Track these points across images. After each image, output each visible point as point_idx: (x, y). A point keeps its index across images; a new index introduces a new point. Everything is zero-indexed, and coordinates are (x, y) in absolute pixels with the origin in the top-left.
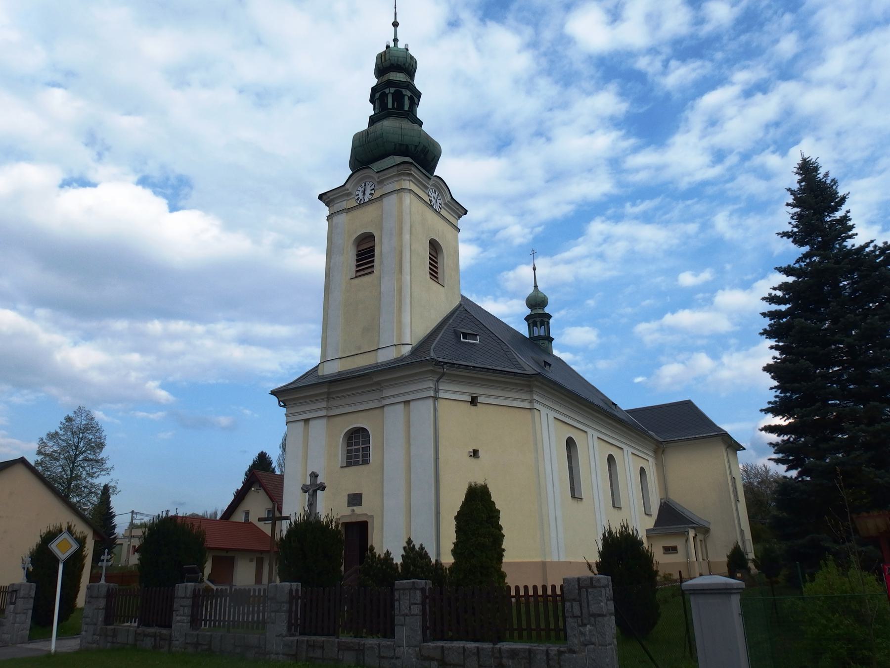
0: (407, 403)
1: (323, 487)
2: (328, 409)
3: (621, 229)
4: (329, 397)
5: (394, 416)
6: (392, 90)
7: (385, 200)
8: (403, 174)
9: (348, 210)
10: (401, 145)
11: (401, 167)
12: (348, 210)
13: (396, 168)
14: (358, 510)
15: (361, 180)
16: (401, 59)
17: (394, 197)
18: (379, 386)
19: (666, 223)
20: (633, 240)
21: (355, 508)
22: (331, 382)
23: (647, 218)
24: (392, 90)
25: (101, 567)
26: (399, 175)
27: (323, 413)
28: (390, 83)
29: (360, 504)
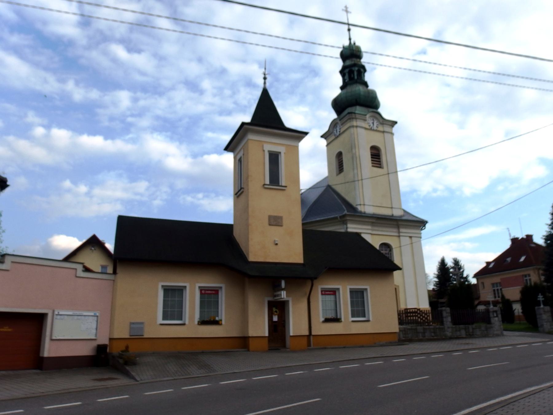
0: (411, 237)
4: (373, 224)
9: (366, 129)
12: (366, 129)
19: (36, 65)
23: (16, 51)
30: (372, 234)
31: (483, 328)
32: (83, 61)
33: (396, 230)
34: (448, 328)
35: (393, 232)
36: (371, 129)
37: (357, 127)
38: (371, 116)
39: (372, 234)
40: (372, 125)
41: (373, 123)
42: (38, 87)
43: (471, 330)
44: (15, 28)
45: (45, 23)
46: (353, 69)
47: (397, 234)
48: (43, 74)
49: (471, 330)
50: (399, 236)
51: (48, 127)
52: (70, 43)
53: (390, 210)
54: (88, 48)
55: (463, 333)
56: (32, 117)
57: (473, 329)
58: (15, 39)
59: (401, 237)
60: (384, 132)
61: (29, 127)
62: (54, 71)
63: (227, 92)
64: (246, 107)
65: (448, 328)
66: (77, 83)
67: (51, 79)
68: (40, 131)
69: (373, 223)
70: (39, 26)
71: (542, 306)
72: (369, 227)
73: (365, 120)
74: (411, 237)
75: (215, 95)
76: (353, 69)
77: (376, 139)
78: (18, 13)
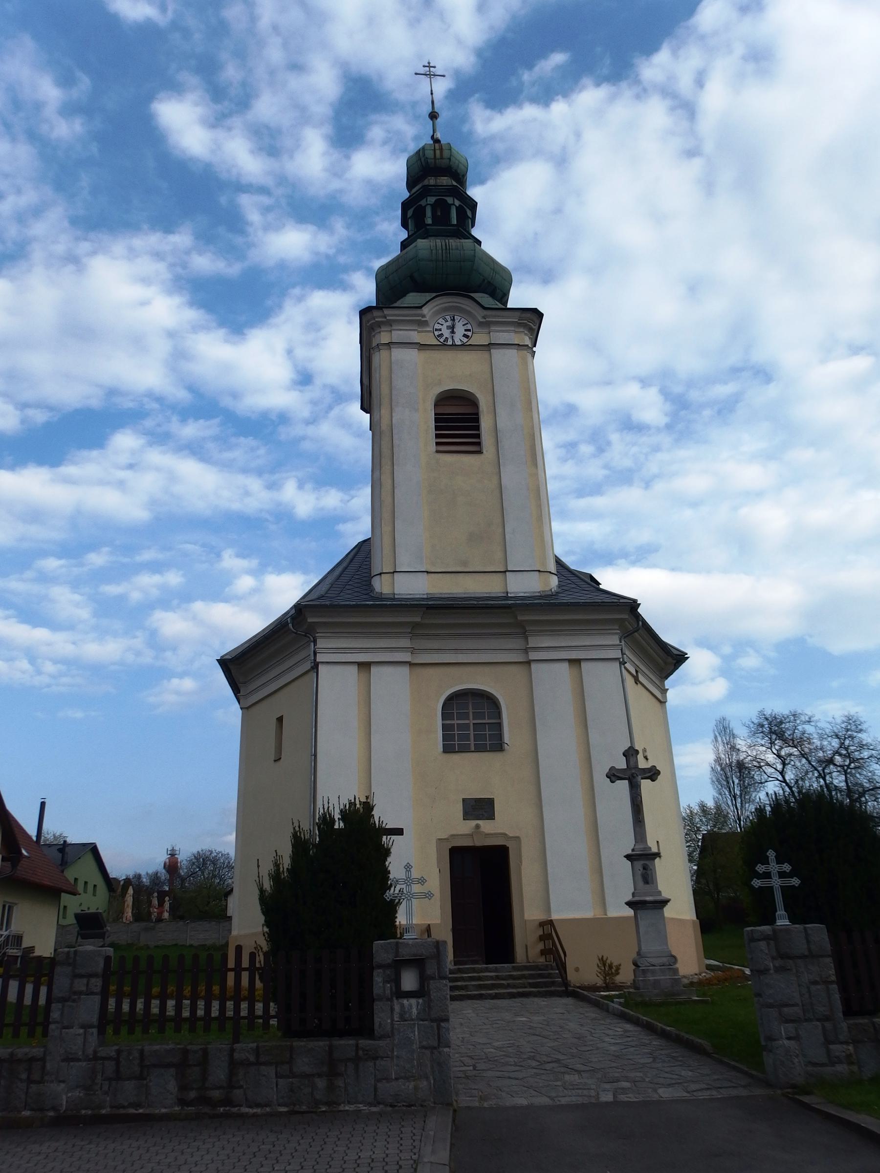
0: (575, 663)
1: (613, 775)
2: (413, 650)
3: (156, 457)
4: (415, 631)
5: (552, 681)
6: (432, 200)
7: (497, 354)
8: (525, 326)
9: (422, 347)
10: (489, 283)
11: (528, 315)
12: (422, 347)
13: (518, 314)
14: (486, 826)
15: (446, 310)
16: (461, 166)
17: (512, 353)
18: (523, 631)
19: (226, 466)
20: (172, 477)
21: (480, 822)
22: (429, 607)
23: (194, 450)
24: (432, 200)
25: (779, 861)
26: (519, 325)
27: (406, 657)
28: (426, 191)
29: (491, 816)
30: (410, 664)
31: (303, 1064)
32: (306, 445)
33: (518, 643)
34: (69, 1059)
35: (504, 650)
36: (444, 346)
37: (389, 345)
38: (437, 313)
39: (410, 664)
40: (446, 333)
41: (452, 329)
42: (236, 506)
43: (219, 1073)
44: (187, 413)
45: (235, 395)
46: (423, 203)
47: (520, 658)
48: (241, 480)
49: (219, 1073)
50: (528, 663)
51: (258, 572)
52: (283, 418)
53: (498, 578)
54: (312, 421)
55: (164, 1089)
56: (230, 561)
57: (234, 1065)
58: (191, 430)
59: (534, 666)
60: (490, 346)
61: (228, 578)
62: (259, 472)
63: (586, 449)
64: (630, 471)
65: (69, 1059)
66: (301, 486)
67: (255, 484)
68: (246, 583)
69: (415, 626)
70: (227, 402)
71: (782, 921)
72: (405, 642)
73: (423, 323)
74: (575, 663)
75: (564, 460)
76: (423, 203)
77: (460, 372)
78: (191, 388)
